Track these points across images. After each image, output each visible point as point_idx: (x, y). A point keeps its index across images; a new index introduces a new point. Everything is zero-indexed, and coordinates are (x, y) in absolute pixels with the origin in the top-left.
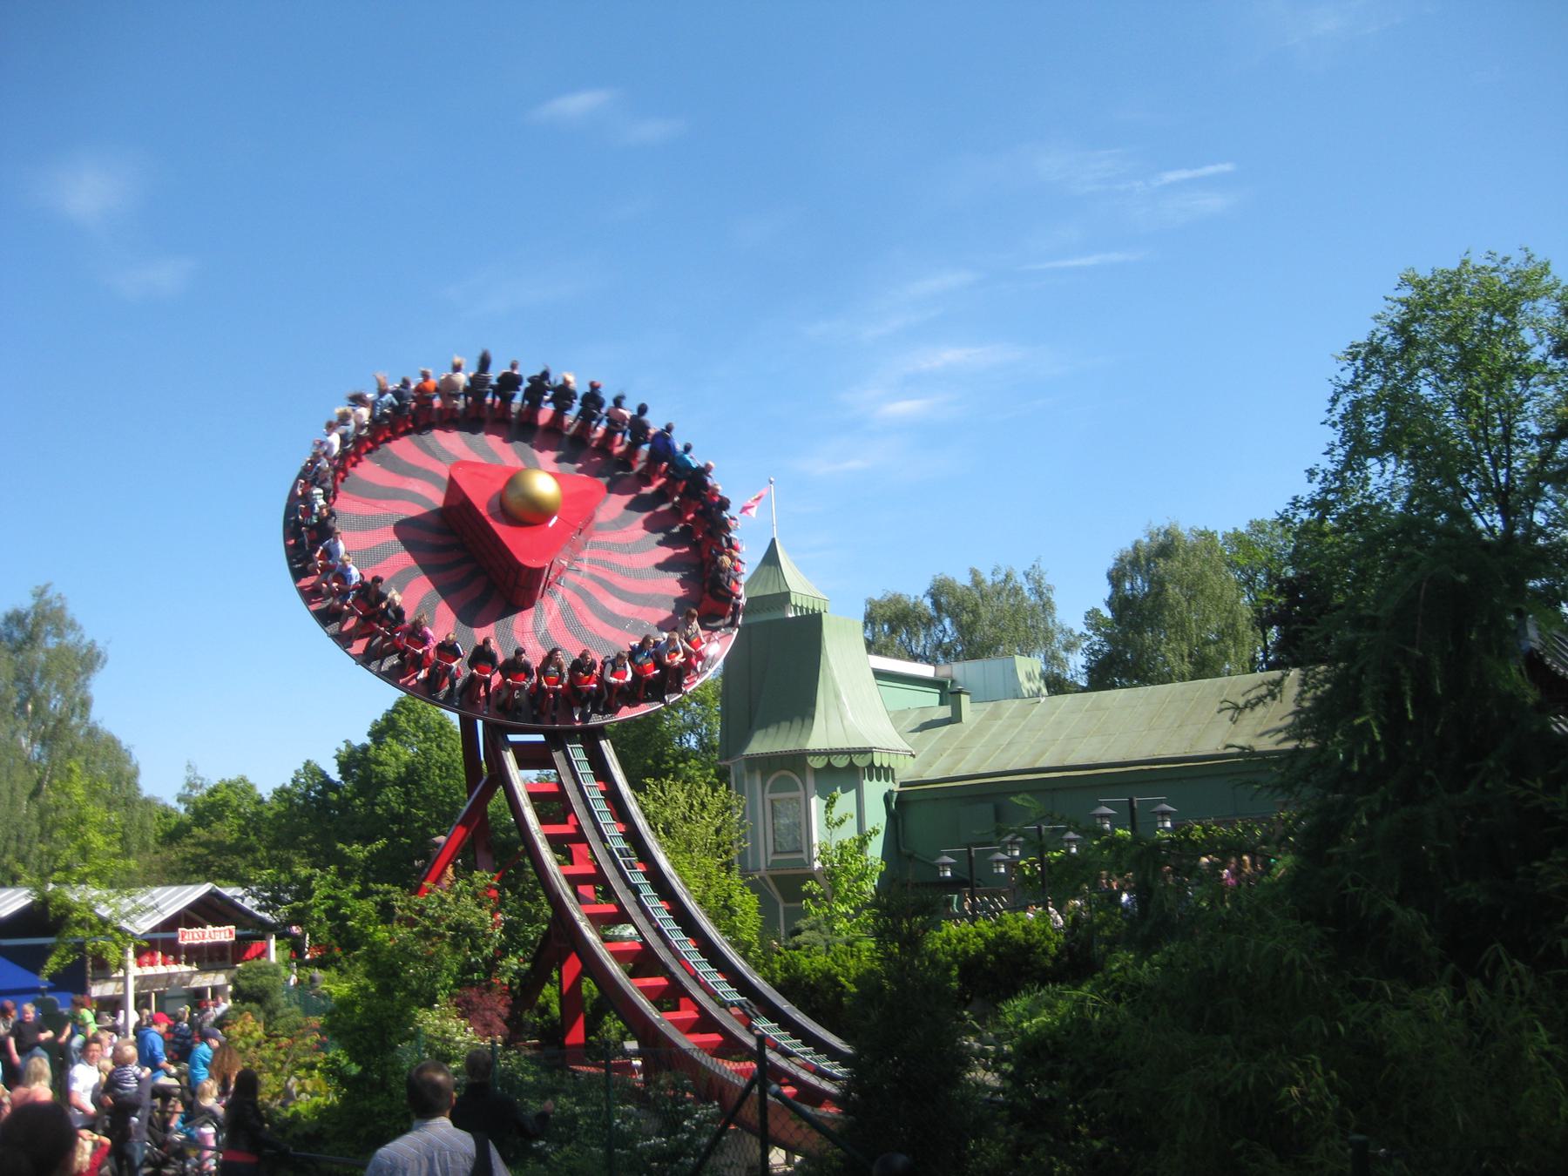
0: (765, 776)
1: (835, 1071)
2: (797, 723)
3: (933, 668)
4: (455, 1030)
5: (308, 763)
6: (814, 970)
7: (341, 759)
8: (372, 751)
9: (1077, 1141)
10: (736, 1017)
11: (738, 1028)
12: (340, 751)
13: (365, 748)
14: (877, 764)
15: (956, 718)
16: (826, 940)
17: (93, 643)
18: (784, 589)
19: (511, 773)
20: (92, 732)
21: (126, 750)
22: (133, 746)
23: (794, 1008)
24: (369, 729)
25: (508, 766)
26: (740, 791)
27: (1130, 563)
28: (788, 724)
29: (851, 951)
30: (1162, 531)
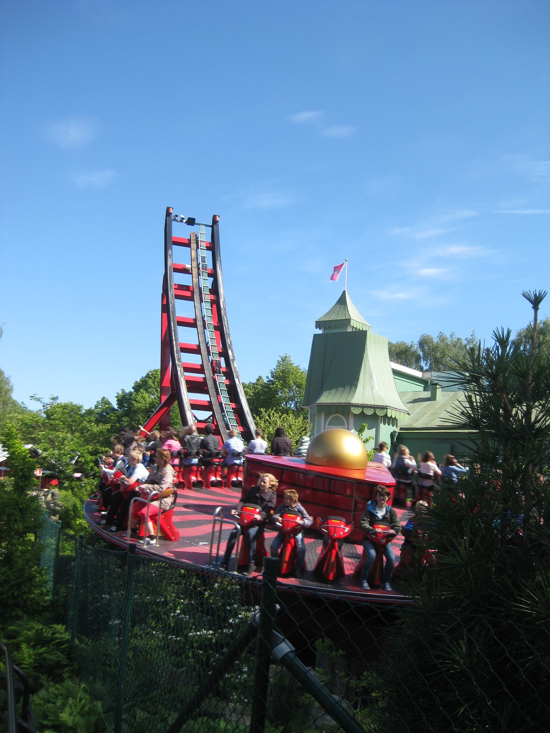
0: (327, 415)
2: (347, 389)
3: (421, 373)
5: (103, 398)
7: (119, 398)
8: (134, 395)
12: (119, 394)
13: (131, 394)
14: (389, 416)
15: (433, 398)
18: (348, 317)
19: (182, 392)
21: (7, 378)
22: (11, 376)
24: (133, 385)
25: (182, 388)
26: (312, 421)
27: (525, 336)
28: (343, 389)
30: (543, 322)
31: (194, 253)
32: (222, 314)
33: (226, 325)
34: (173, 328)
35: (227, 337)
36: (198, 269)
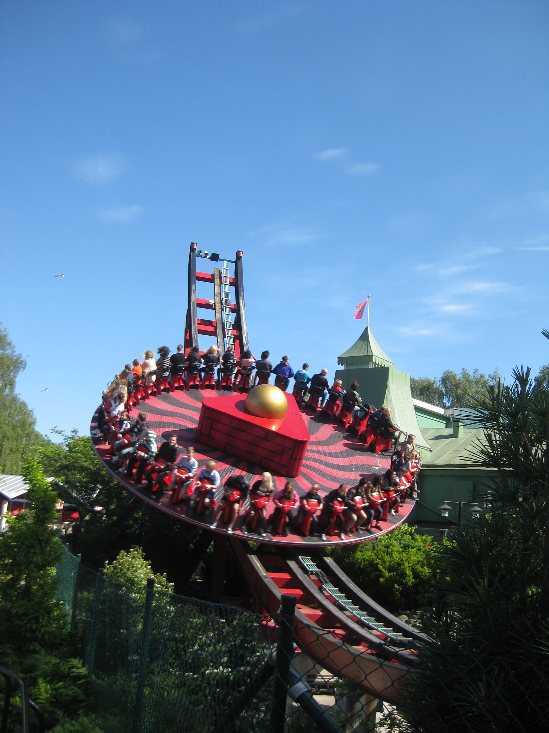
1: (371, 624)
4: (140, 566)
6: (364, 559)
9: (75, 471)
10: (313, 581)
11: (313, 588)
15: (455, 435)
16: (373, 543)
17: (20, 355)
18: (370, 354)
20: (14, 400)
21: (31, 411)
23: (350, 580)
29: (387, 551)
31: (217, 288)
36: (222, 304)
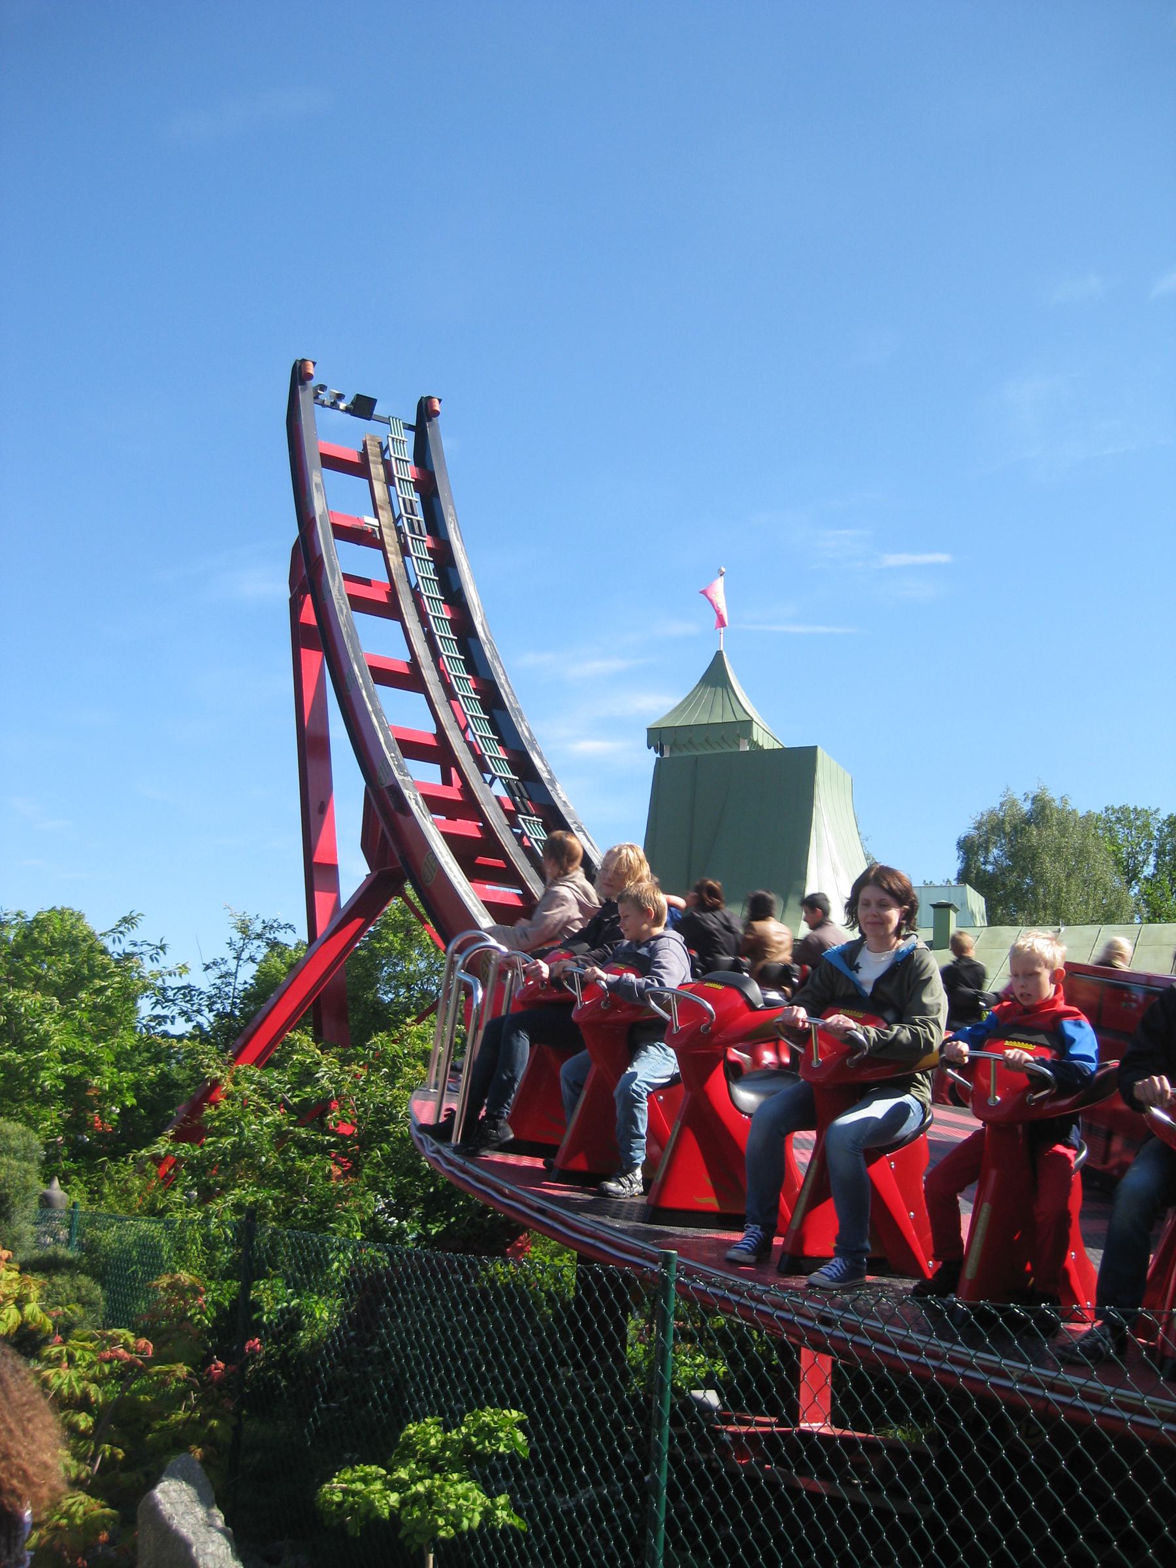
18: (742, 717)
31: (379, 488)
32: (488, 654)
33: (506, 686)
34: (361, 681)
35: (516, 716)
36: (399, 531)
